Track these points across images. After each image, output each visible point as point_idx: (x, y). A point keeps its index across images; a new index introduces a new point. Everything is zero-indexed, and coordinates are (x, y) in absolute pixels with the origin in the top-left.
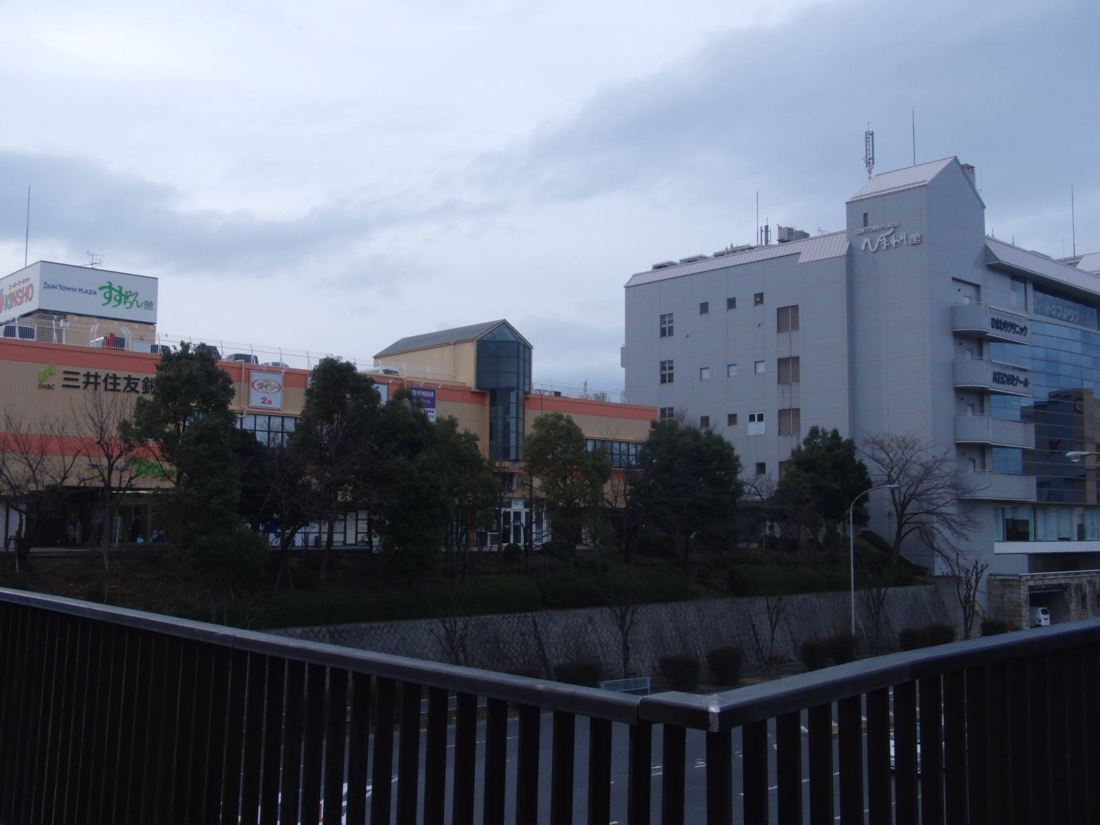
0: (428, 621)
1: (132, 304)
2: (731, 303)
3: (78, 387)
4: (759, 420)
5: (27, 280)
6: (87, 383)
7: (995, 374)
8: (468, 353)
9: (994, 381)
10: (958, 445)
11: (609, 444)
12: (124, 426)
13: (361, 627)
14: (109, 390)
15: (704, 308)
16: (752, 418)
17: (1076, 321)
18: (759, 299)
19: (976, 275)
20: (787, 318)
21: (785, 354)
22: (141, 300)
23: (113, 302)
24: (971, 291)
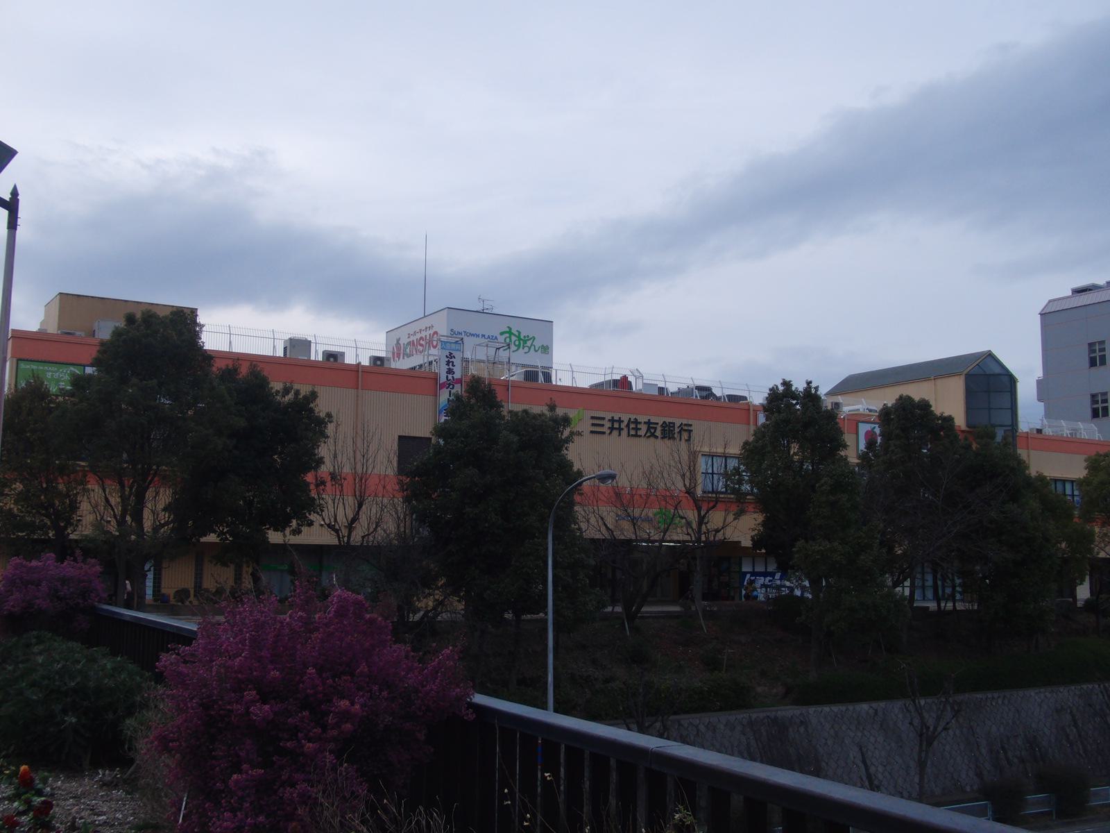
0: (1036, 691)
1: (530, 348)
3: (604, 433)
4: (1103, 416)
6: (612, 429)
11: (1059, 486)
13: (977, 698)
14: (632, 435)
22: (538, 344)
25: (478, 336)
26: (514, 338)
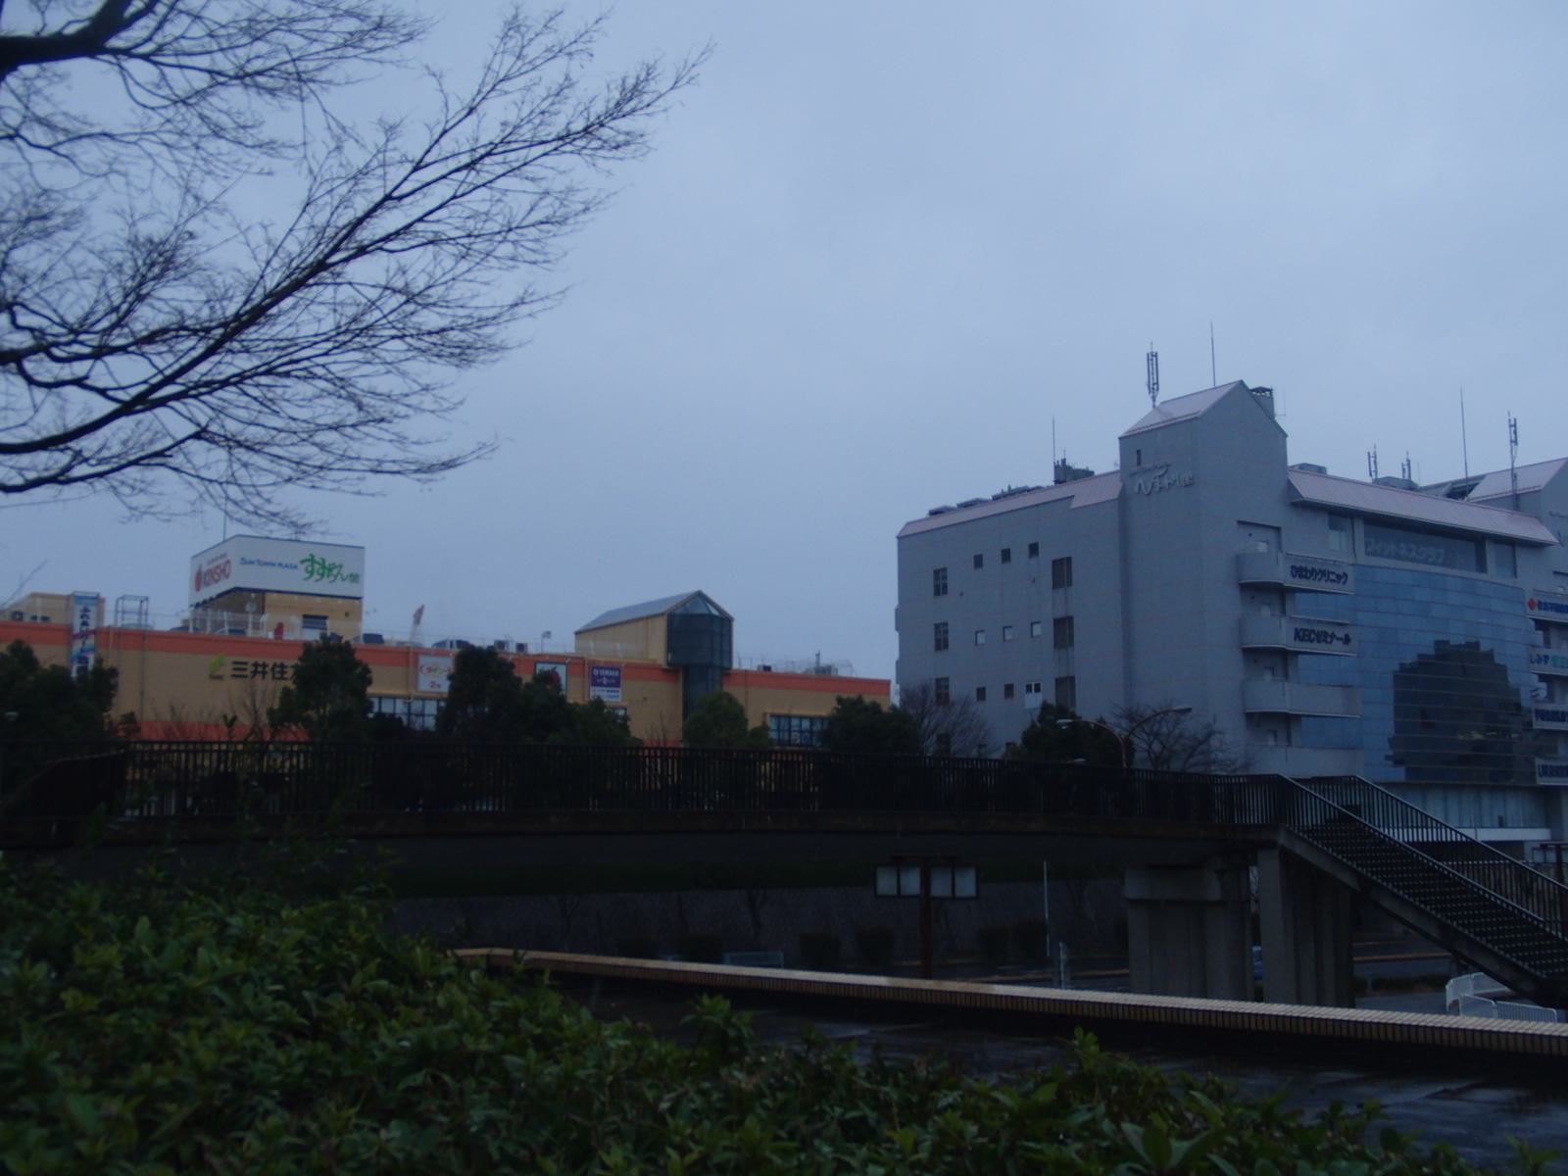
1: (336, 577)
2: (1006, 555)
3: (246, 677)
5: (223, 556)
6: (255, 673)
7: (1297, 632)
8: (659, 631)
9: (1295, 639)
10: (1250, 716)
12: (271, 712)
15: (978, 561)
16: (1029, 688)
17: (1440, 560)
18: (1034, 549)
19: (1277, 516)
20: (1062, 572)
21: (1060, 614)
22: (345, 572)
23: (316, 576)
24: (1271, 535)
25: (273, 565)
26: (317, 567)
